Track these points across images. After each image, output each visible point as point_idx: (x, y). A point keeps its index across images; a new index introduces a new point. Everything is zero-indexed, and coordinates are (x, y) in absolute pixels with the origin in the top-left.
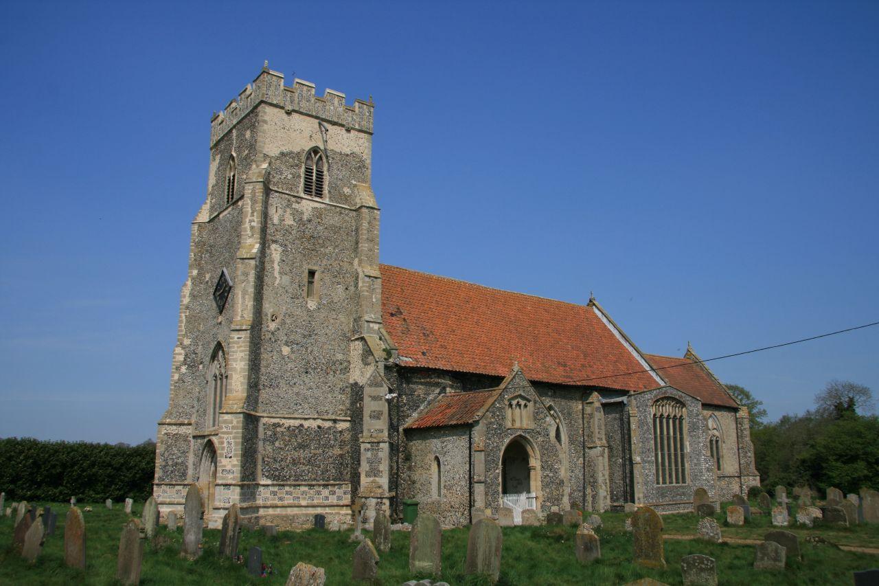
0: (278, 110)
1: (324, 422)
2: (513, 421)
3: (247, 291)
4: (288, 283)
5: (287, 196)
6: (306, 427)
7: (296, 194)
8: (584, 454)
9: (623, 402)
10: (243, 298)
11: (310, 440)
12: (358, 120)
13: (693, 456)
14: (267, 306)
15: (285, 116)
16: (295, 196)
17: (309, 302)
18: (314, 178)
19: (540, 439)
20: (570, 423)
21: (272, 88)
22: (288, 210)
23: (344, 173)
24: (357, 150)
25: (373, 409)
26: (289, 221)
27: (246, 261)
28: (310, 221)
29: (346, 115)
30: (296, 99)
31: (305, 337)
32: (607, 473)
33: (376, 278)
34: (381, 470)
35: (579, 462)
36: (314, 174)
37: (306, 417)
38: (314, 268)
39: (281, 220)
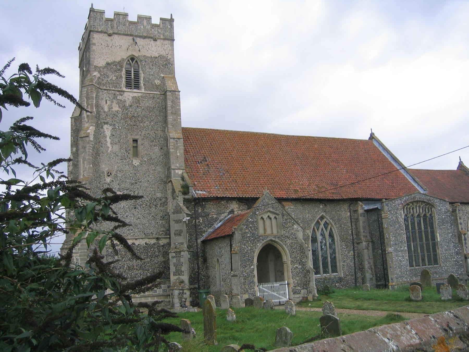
0: (103, 34)
1: (150, 240)
2: (265, 229)
3: (85, 158)
4: (117, 150)
5: (113, 92)
6: (137, 244)
7: (120, 90)
8: (354, 248)
9: (377, 208)
10: (84, 163)
11: (140, 253)
12: (162, 32)
13: (443, 244)
14: (104, 166)
15: (107, 38)
16: (119, 91)
17: (134, 160)
18: (133, 77)
19: (289, 242)
20: (341, 226)
21: (98, 21)
22: (114, 101)
23: (154, 70)
24: (163, 53)
25: (176, 229)
26: (116, 108)
27: (84, 138)
28: (131, 106)
29: (153, 30)
30: (115, 25)
31: (132, 184)
32: (372, 261)
33: (179, 139)
34: (182, 270)
35: (350, 254)
36: (133, 74)
37: (136, 238)
38: (136, 137)
39: (110, 108)
